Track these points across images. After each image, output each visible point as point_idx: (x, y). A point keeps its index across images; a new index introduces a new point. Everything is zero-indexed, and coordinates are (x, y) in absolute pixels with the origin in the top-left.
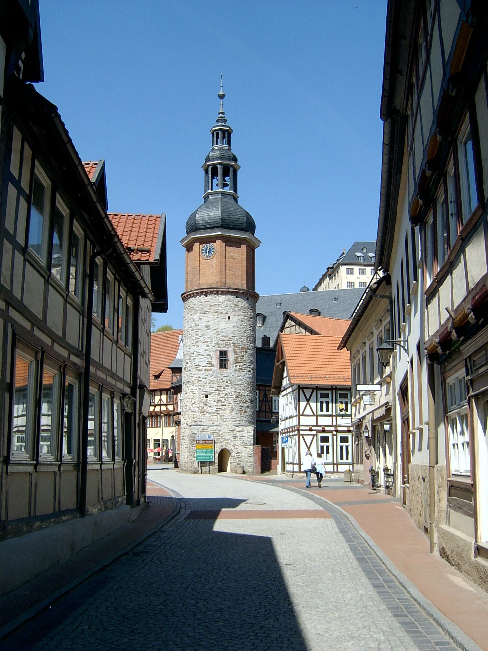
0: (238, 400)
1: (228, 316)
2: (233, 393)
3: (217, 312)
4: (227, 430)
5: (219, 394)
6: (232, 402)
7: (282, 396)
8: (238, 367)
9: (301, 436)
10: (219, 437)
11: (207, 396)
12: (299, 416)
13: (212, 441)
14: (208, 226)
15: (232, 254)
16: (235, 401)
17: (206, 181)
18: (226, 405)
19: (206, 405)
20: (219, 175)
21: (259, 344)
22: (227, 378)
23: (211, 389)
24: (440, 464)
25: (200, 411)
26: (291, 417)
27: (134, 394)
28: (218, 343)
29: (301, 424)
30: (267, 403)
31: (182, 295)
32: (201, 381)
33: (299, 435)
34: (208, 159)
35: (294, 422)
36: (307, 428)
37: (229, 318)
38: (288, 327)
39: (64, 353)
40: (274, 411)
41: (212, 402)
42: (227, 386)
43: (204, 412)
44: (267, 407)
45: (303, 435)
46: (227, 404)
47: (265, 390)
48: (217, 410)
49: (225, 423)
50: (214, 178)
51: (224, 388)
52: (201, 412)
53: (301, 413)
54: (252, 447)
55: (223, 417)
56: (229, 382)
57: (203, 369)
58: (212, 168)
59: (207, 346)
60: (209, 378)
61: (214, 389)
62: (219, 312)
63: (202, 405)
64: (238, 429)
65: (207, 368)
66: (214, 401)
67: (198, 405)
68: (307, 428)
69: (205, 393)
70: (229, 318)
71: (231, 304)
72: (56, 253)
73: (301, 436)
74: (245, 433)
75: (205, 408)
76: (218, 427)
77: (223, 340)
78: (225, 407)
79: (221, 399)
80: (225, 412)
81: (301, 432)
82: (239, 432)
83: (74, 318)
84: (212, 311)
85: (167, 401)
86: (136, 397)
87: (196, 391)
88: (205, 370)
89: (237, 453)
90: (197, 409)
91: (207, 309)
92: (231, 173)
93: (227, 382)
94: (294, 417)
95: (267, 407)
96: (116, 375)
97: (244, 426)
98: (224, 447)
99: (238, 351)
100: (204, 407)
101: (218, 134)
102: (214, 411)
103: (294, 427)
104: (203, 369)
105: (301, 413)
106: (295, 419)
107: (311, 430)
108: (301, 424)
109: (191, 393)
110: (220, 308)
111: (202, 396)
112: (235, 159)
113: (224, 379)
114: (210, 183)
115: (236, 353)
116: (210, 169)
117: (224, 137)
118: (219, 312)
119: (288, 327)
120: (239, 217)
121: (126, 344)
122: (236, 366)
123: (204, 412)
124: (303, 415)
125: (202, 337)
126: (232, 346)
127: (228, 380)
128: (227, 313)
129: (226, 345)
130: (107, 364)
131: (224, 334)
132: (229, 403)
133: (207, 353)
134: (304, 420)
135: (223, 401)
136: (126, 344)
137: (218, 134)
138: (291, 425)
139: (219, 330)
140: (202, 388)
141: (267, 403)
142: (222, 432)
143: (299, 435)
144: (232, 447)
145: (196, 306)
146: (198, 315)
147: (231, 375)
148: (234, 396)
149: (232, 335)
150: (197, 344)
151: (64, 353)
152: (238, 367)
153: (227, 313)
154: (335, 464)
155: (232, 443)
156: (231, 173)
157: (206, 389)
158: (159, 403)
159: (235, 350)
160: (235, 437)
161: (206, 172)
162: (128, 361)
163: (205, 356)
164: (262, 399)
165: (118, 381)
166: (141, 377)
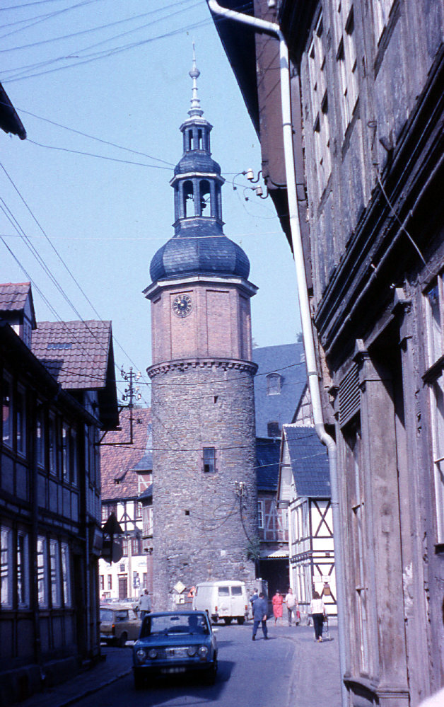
7: (292, 510)
9: (315, 566)
12: (311, 538)
14: (181, 269)
17: (176, 203)
20: (195, 193)
21: (263, 434)
24: (172, 621)
26: (303, 540)
27: (82, 533)
29: (314, 549)
31: (147, 370)
33: (312, 564)
34: (178, 170)
35: (305, 546)
36: (323, 554)
38: (307, 404)
39: (16, 510)
45: (317, 564)
50: (188, 198)
53: (314, 535)
58: (184, 184)
68: (323, 554)
72: (6, 436)
73: (315, 566)
81: (315, 561)
83: (22, 472)
85: (135, 517)
86: (85, 537)
92: (213, 189)
94: (306, 539)
96: (63, 517)
101: (191, 132)
103: (305, 553)
105: (314, 535)
106: (307, 542)
107: (328, 557)
108: (314, 549)
112: (216, 169)
114: (182, 205)
116: (181, 184)
117: (200, 136)
119: (307, 404)
120: (224, 254)
121: (72, 480)
124: (316, 537)
130: (53, 508)
134: (318, 544)
136: (72, 480)
137: (191, 132)
138: (302, 552)
143: (312, 564)
151: (16, 510)
156: (213, 189)
158: (123, 520)
161: (177, 189)
162: (75, 499)
165: (66, 523)
166: (91, 512)
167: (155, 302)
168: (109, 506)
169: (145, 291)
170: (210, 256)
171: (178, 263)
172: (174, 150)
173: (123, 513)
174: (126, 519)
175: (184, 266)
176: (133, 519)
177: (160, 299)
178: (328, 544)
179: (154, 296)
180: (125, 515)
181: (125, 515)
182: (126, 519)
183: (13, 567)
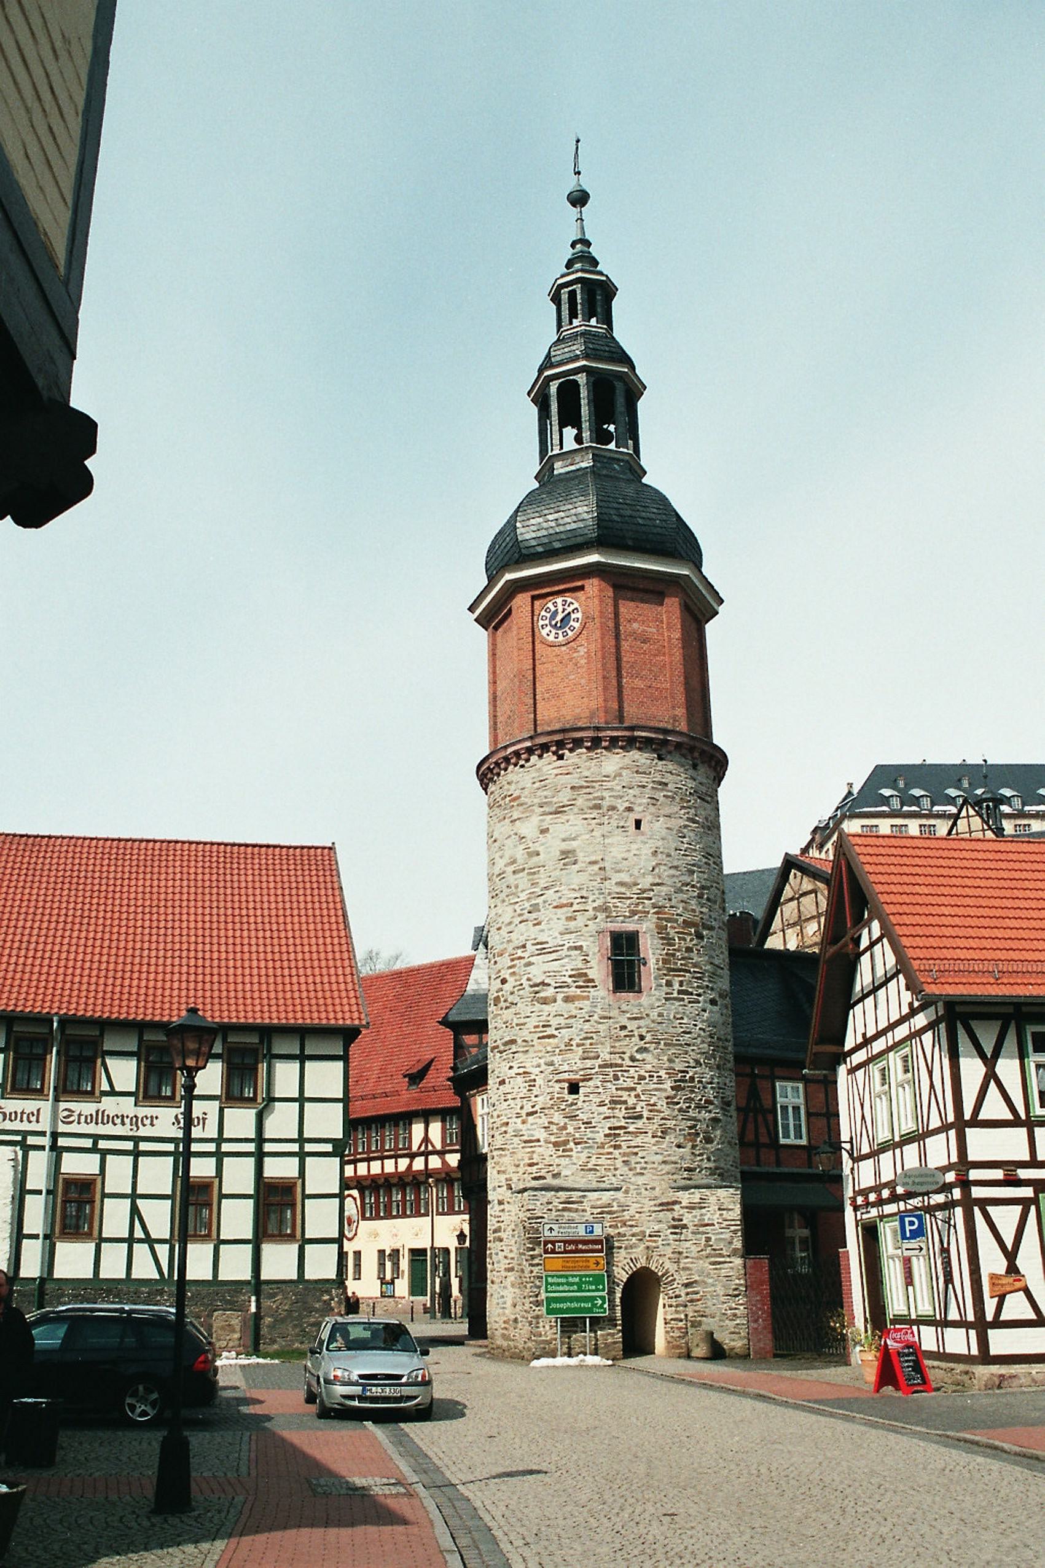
0: (681, 1097)
1: (633, 816)
2: (662, 1073)
3: (598, 807)
4: (649, 1205)
5: (616, 1078)
6: (662, 1104)
8: (676, 986)
10: (622, 1230)
11: (574, 1088)
13: (600, 1242)
14: (557, 545)
15: (635, 625)
16: (671, 1101)
18: (640, 1117)
19: (573, 1117)
22: (642, 1023)
23: (589, 1063)
25: (553, 1139)
28: (604, 909)
30: (760, 1118)
32: (554, 1036)
36: (998, 1174)
37: (638, 824)
40: (782, 1141)
41: (594, 1108)
42: (641, 1050)
43: (566, 1142)
44: (763, 1130)
45: (984, 1203)
46: (645, 1114)
47: (753, 1076)
48: (614, 1133)
49: (640, 1180)
51: (633, 1059)
52: (556, 1144)
54: (738, 1261)
55: (633, 1159)
56: (648, 1038)
57: (560, 997)
59: (569, 919)
60: (578, 1024)
61: (600, 1061)
62: (605, 804)
63: (558, 1118)
64: (685, 1197)
65: (573, 991)
66: (602, 1104)
67: (544, 1121)
68: (998, 1174)
69: (566, 1076)
70: (638, 824)
71: (644, 780)
74: (711, 1214)
75: (570, 1129)
76: (619, 1195)
77: (621, 897)
78: (640, 1124)
79: (625, 1095)
80: (638, 1141)
81: (977, 1192)
82: (691, 1208)
84: (580, 802)
87: (537, 1071)
88: (567, 999)
89: (686, 1285)
90: (542, 1135)
93: (642, 1038)
95: (763, 1130)
97: (708, 1187)
98: (642, 1263)
99: (672, 932)
100: (565, 1128)
102: (600, 1138)
104: (560, 997)
107: (1011, 1181)
109: (520, 1079)
110: (606, 794)
111: (557, 1085)
113: (632, 1025)
115: (668, 941)
118: (605, 804)
119: (791, 899)
122: (669, 984)
123: (566, 1142)
125: (551, 891)
126: (653, 918)
127: (643, 1031)
128: (629, 809)
129: (634, 913)
131: (624, 877)
133: (571, 940)
134: (983, 1144)
135: (631, 1101)
139: (606, 864)
140: (557, 1059)
141: (760, 1118)
142: (632, 1211)
143: (968, 1203)
144: (668, 1265)
145: (526, 792)
146: (535, 820)
147: (654, 1015)
148: (668, 1085)
149: (650, 879)
150: (534, 915)
152: (676, 986)
153: (629, 809)
154: (301, 1147)
155: (668, 1251)
157: (573, 1064)
159: (661, 929)
160: (678, 1226)
163: (565, 952)
164: (743, 1104)
167: (496, 628)
168: (397, 1125)
169: (471, 609)
170: (620, 516)
171: (551, 531)
172: (535, 333)
173: (422, 1135)
174: (426, 1146)
175: (563, 536)
176: (439, 1147)
177: (510, 611)
178: (1011, 1145)
179: (493, 616)
180: (426, 1140)
181: (426, 1140)
182: (426, 1146)
183: (786, 1407)
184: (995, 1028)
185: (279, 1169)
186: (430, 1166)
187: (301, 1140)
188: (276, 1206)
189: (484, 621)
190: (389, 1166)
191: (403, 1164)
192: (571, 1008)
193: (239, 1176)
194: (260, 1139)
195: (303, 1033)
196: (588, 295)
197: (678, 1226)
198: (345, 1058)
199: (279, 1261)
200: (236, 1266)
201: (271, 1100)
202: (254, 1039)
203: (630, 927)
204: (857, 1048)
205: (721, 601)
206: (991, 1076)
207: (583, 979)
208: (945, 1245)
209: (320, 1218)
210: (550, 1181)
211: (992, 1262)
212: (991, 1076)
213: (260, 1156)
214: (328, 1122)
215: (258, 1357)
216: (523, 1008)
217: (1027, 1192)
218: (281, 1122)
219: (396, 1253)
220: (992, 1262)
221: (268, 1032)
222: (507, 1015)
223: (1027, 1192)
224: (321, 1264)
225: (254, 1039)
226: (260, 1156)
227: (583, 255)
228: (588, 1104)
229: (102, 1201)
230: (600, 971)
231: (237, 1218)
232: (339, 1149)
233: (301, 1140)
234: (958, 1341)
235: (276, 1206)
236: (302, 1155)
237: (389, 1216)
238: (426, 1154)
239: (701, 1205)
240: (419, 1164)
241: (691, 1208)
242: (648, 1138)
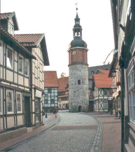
36: (101, 100)
45: (100, 102)
70: (80, 71)
91: (74, 68)
115: (83, 80)
132: (81, 94)
148: (82, 92)
157: (75, 90)
181: (67, 94)
184: (102, 89)
185: (53, 98)
186: (49, 101)
187: (54, 96)
188: (53, 101)
189: (68, 52)
190: (64, 96)
191: (65, 96)
192: (75, 86)
193: (49, 99)
194: (51, 96)
195: (54, 87)
196: (77, 20)
197: (83, 103)
198: (57, 89)
199: (53, 105)
200: (49, 106)
201: (51, 93)
202: (50, 88)
203: (79, 79)
204: (97, 90)
205: (88, 50)
206: (101, 93)
207: (76, 83)
208: (5, 99)
209: (56, 102)
210: (73, 99)
211: (100, 106)
212: (101, 93)
213: (51, 97)
214: (56, 94)
215: (54, 128)
216: (71, 86)
217: (103, 101)
218: (52, 94)
219: (64, 104)
220: (100, 106)
221: (51, 87)
222: (70, 86)
223: (103, 101)
224: (56, 105)
225: (50, 88)
226: (51, 97)
227: (77, 16)
228: (76, 93)
229: (100, 112)
230: (77, 83)
231: (49, 102)
232: (57, 96)
233: (54, 96)
234: (98, 111)
235: (53, 101)
236: (54, 97)
237: (64, 100)
238: (67, 95)
239: (85, 101)
240: (66, 96)
241: (84, 101)
242: (81, 96)
